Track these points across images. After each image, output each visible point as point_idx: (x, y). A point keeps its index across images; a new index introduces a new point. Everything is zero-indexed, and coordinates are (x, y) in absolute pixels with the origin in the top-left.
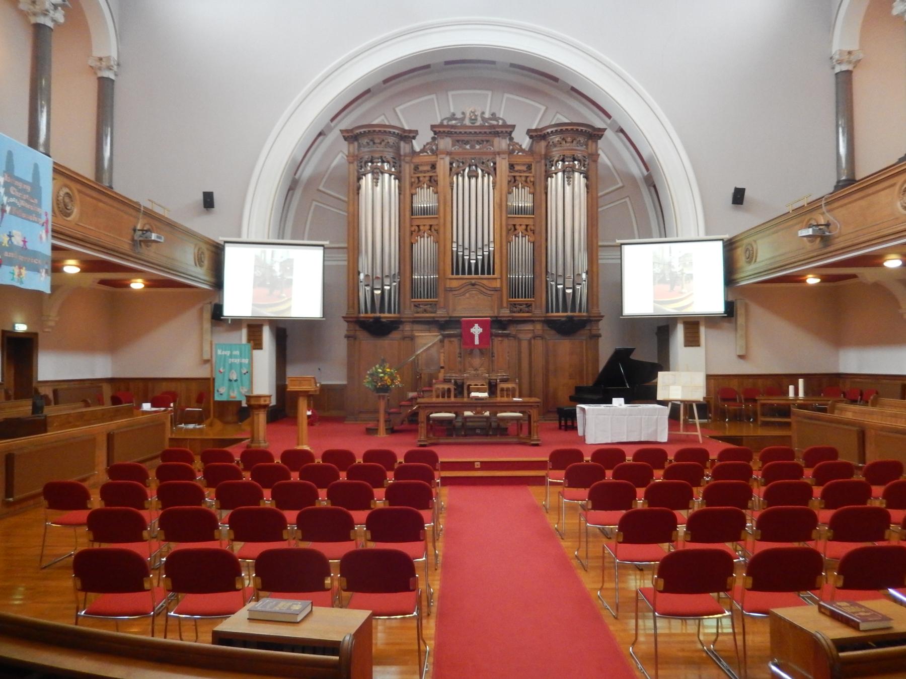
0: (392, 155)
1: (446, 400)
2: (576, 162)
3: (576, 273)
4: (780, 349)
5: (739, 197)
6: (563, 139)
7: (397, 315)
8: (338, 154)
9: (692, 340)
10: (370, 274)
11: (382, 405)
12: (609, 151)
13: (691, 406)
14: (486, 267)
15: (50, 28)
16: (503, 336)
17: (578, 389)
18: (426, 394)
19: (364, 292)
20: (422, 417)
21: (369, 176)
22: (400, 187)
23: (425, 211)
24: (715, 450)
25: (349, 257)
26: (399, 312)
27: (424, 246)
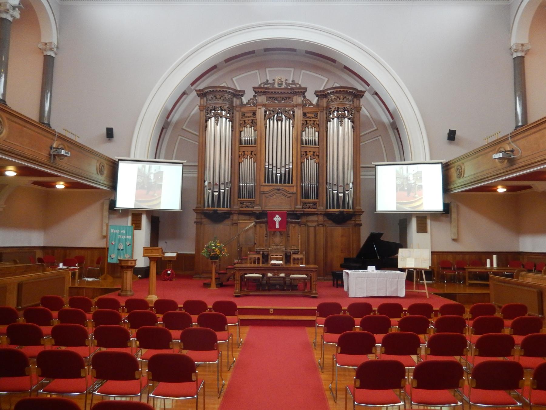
0: (228, 106)
1: (256, 265)
2: (346, 112)
3: (346, 183)
4: (479, 236)
5: (452, 136)
6: (338, 97)
7: (228, 209)
8: (192, 105)
9: (422, 229)
10: (211, 181)
11: (214, 267)
12: (368, 106)
13: (421, 272)
14: (287, 178)
15: (10, 21)
16: (296, 223)
17: (346, 260)
18: (244, 261)
19: (207, 193)
20: (238, 277)
21: (213, 118)
22: (232, 127)
23: (248, 142)
24: (437, 303)
25: (198, 171)
26: (230, 207)
27: (247, 165)
